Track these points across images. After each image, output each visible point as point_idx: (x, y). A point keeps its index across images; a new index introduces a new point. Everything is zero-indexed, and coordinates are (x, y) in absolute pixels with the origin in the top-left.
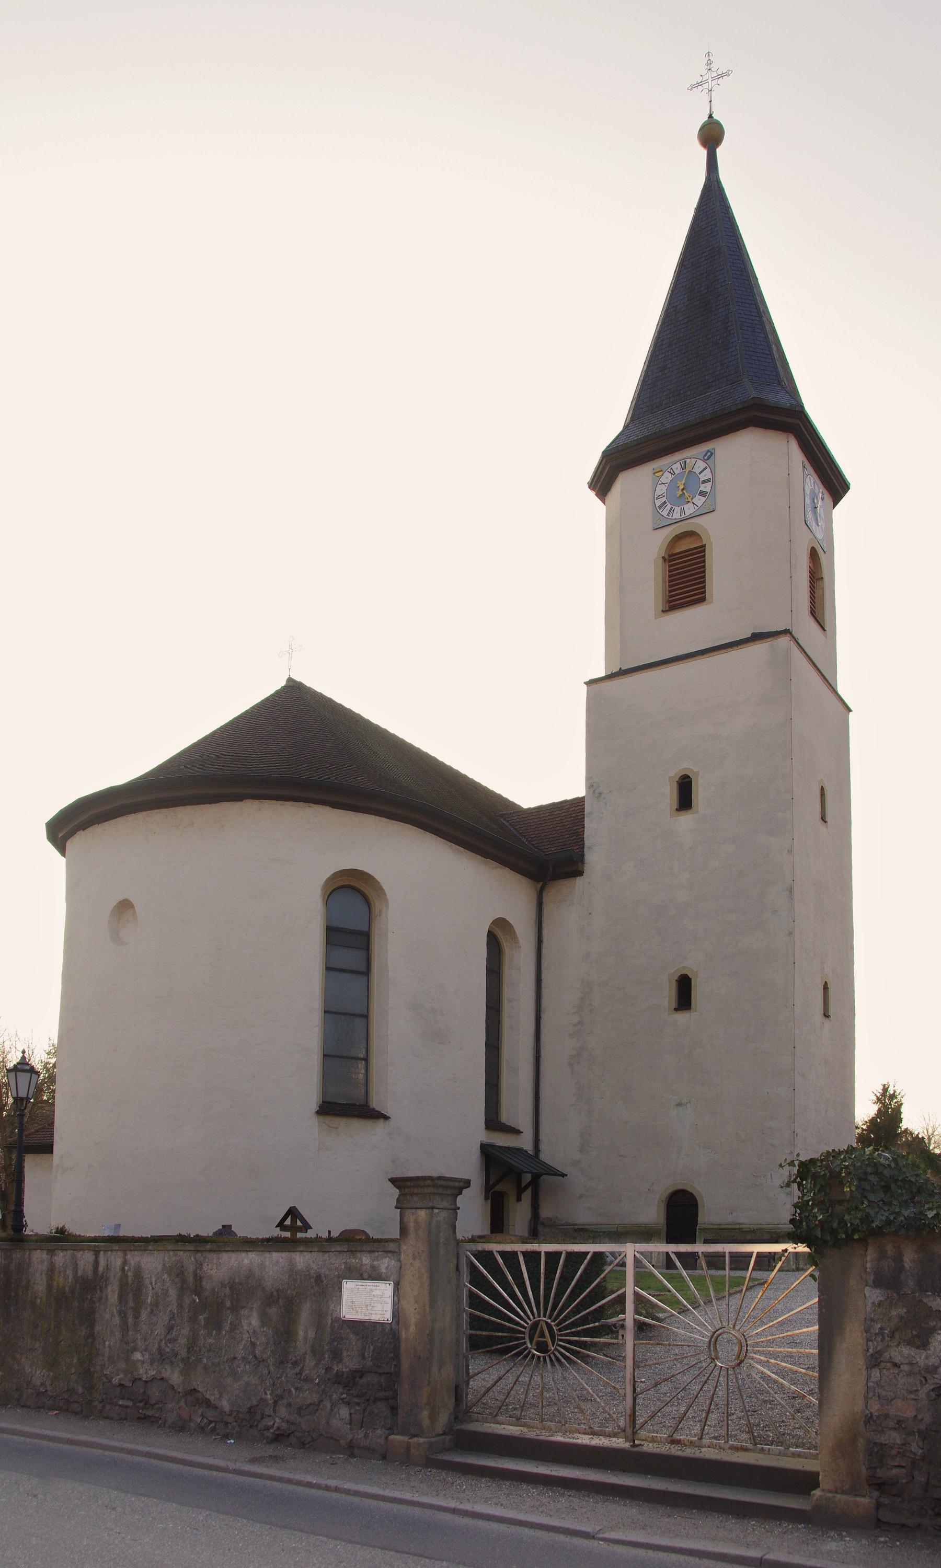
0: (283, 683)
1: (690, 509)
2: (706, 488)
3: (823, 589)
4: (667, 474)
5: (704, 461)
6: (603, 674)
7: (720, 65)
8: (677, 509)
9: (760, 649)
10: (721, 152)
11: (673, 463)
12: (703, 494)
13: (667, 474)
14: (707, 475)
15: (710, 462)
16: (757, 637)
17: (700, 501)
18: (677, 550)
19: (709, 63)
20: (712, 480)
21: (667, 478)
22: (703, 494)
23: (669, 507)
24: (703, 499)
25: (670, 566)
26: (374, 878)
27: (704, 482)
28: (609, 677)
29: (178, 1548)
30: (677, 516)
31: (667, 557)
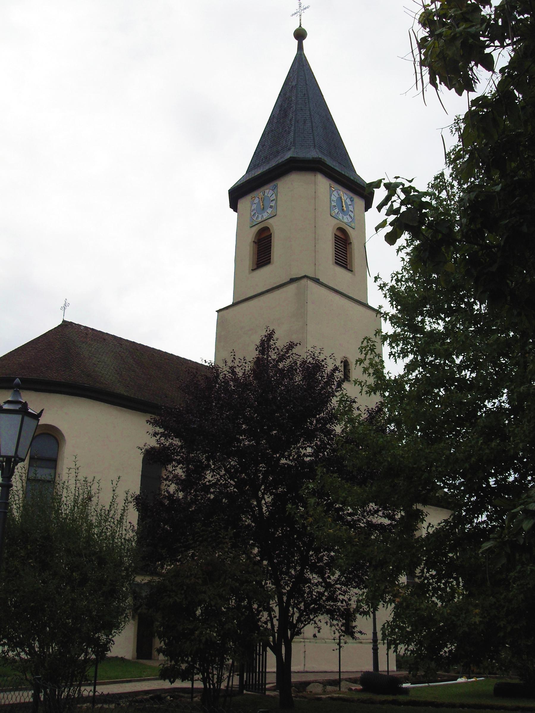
0: (60, 322)
1: (265, 215)
2: (273, 204)
3: (351, 248)
4: (257, 199)
5: (273, 190)
6: (230, 302)
7: (304, 5)
8: (260, 216)
9: (292, 287)
10: (306, 43)
11: (258, 194)
12: (271, 207)
13: (257, 199)
14: (274, 197)
15: (275, 191)
16: (293, 281)
17: (269, 211)
18: (263, 236)
19: (300, 4)
20: (276, 200)
21: (256, 201)
22: (271, 207)
23: (257, 215)
24: (271, 209)
25: (258, 245)
26: (58, 429)
27: (272, 201)
28: (234, 305)
29: (437, 467)
30: (260, 220)
31: (256, 241)
